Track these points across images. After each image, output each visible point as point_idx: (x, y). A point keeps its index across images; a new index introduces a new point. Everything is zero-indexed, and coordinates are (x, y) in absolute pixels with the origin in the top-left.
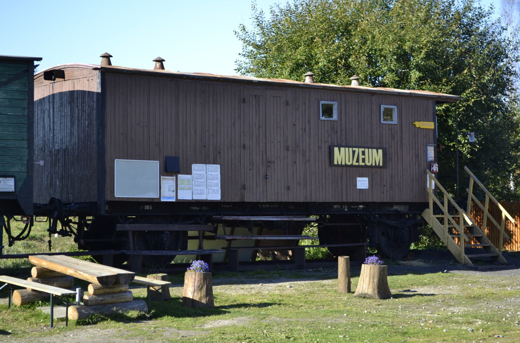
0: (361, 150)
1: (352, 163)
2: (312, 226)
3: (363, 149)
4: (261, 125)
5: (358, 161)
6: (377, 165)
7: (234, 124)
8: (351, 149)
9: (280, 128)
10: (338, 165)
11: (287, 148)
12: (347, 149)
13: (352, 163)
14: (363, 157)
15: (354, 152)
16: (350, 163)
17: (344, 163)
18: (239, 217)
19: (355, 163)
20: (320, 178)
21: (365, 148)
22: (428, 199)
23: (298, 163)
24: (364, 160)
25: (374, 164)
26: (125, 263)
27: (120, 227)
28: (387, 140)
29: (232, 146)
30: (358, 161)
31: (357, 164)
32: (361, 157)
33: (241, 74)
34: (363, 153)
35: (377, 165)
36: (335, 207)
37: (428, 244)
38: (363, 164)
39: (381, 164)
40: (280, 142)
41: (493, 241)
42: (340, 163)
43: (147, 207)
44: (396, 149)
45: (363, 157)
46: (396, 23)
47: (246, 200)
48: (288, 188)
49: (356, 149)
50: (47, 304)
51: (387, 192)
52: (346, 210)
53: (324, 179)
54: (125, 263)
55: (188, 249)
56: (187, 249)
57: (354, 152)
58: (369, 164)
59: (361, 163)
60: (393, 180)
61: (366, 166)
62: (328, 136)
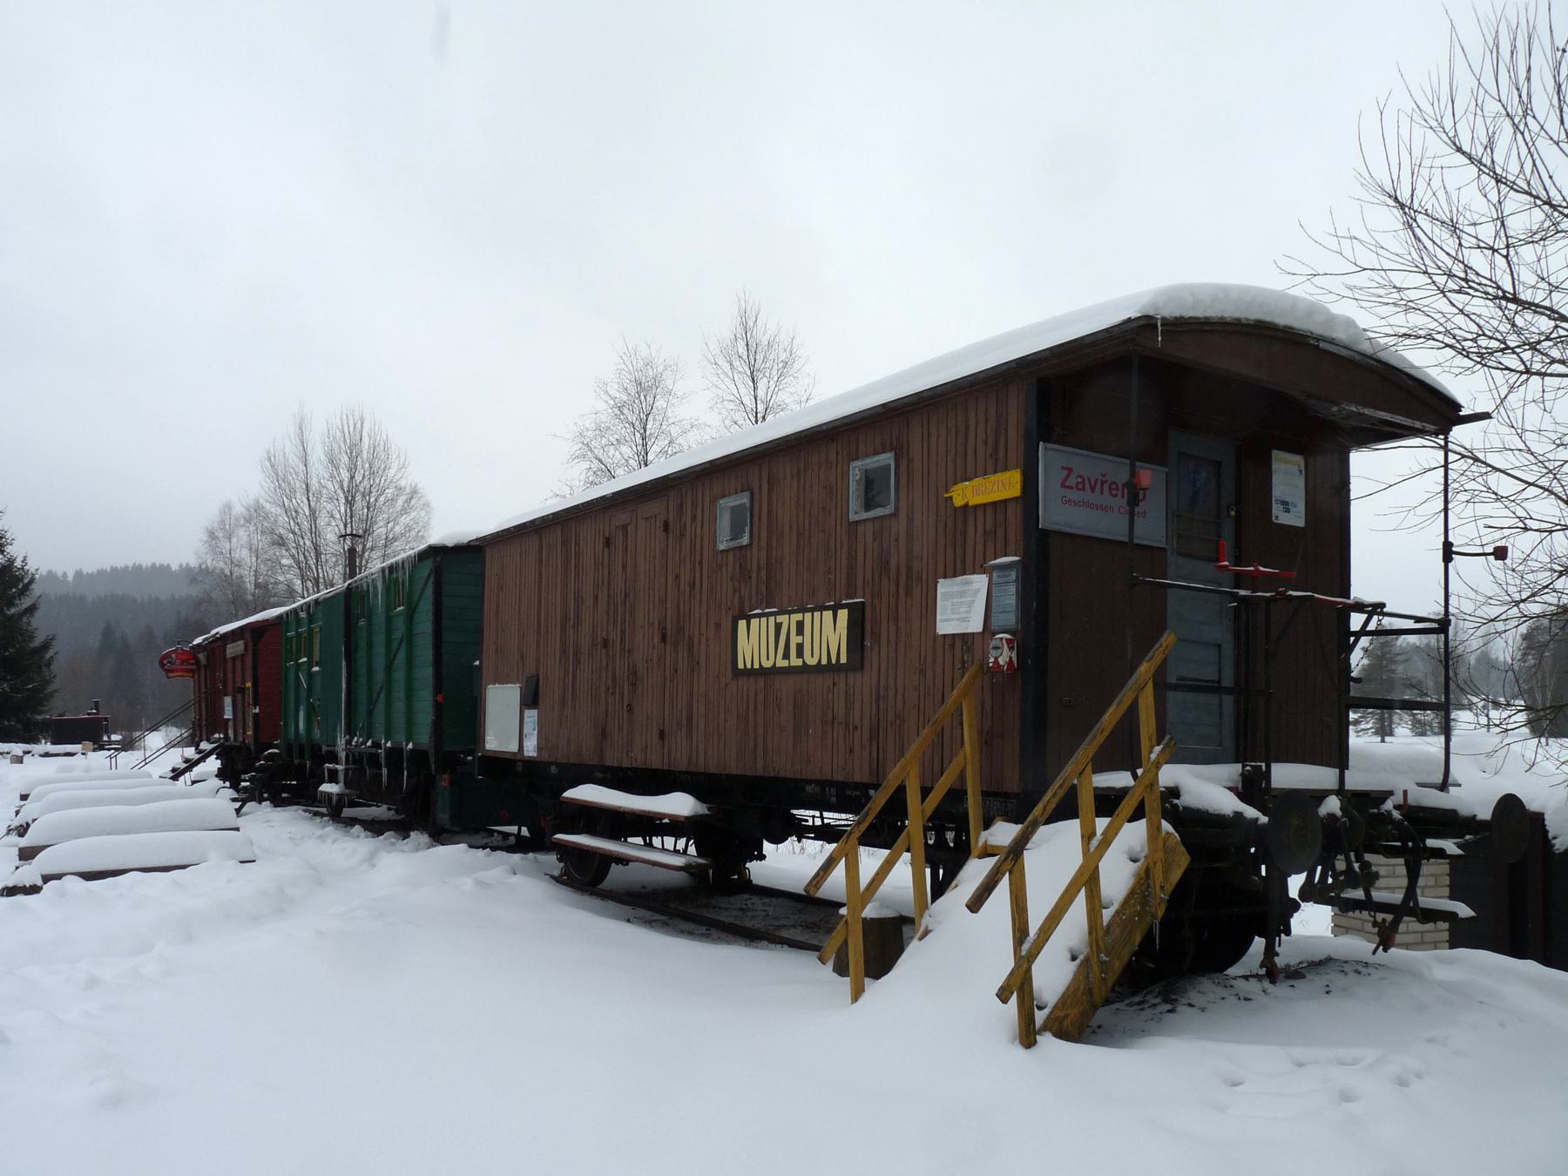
1: (775, 663)
3: (799, 617)
5: (786, 656)
6: (749, 666)
9: (654, 590)
11: (664, 638)
13: (775, 663)
14: (799, 640)
15: (778, 626)
19: (782, 663)
21: (803, 610)
22: (966, 787)
24: (800, 654)
25: (824, 662)
28: (868, 575)
30: (786, 656)
33: (1555, 446)
34: (800, 625)
35: (749, 666)
39: (843, 660)
40: (652, 625)
42: (756, 666)
44: (892, 600)
48: (662, 735)
49: (783, 619)
51: (862, 747)
55: (1097, 819)
56: (1097, 816)
57: (778, 626)
59: (795, 662)
60: (881, 707)
62: (735, 591)
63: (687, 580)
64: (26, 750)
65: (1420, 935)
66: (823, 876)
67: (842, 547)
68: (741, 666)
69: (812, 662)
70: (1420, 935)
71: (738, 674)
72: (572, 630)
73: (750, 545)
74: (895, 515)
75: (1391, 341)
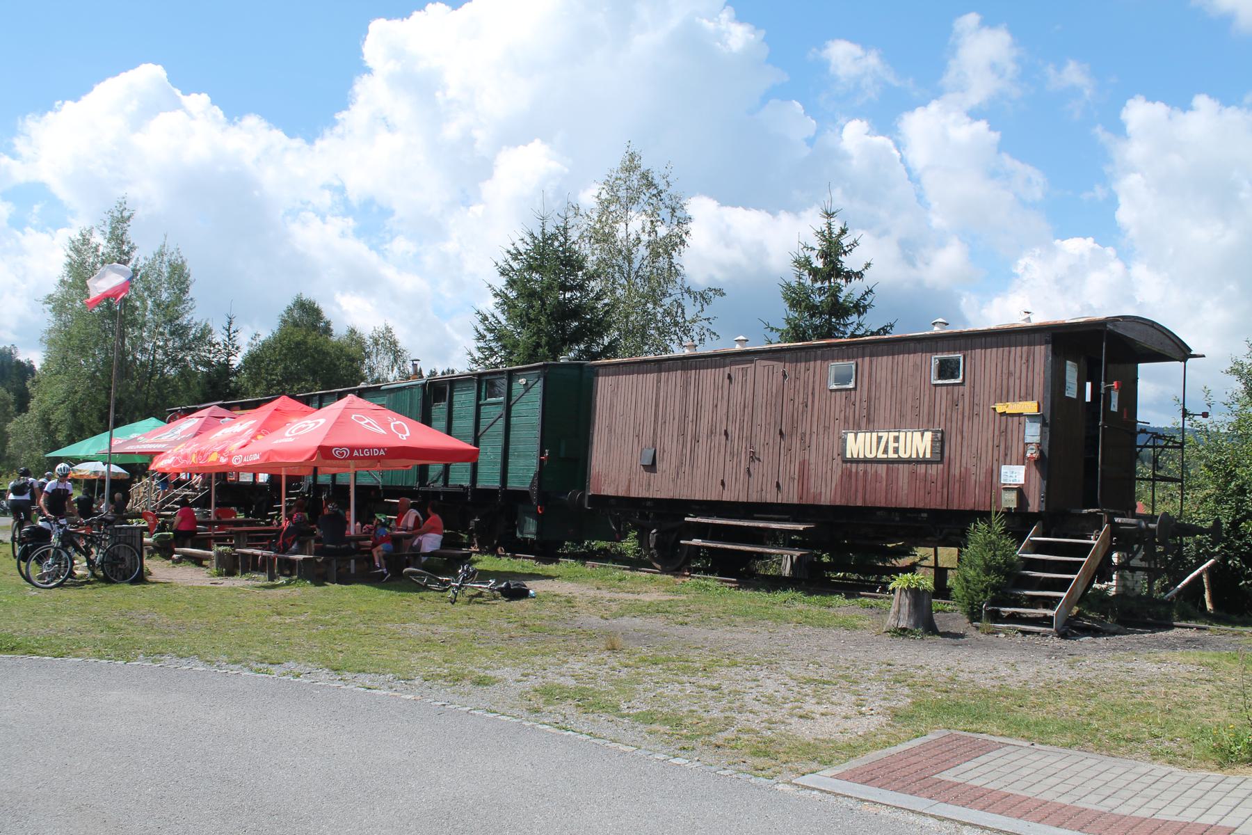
0: (892, 435)
5: (886, 451)
6: (921, 456)
7: (716, 406)
14: (896, 445)
15: (879, 438)
19: (881, 455)
23: (793, 450)
24: (896, 450)
26: (495, 542)
28: (943, 410)
29: (712, 433)
30: (886, 451)
31: (885, 456)
32: (892, 445)
34: (896, 439)
35: (921, 456)
36: (878, 513)
38: (896, 456)
39: (928, 456)
43: (925, 515)
45: (896, 445)
46: (943, 657)
49: (885, 435)
50: (450, 570)
52: (898, 519)
53: (829, 472)
54: (495, 542)
57: (879, 438)
58: (907, 456)
59: (892, 455)
63: (801, 400)
64: (472, 352)
65: (933, 565)
66: (620, 559)
67: (674, 419)
68: (849, 456)
69: (903, 455)
70: (933, 565)
71: (845, 461)
72: (690, 424)
73: (855, 389)
74: (962, 384)
75: (194, 446)
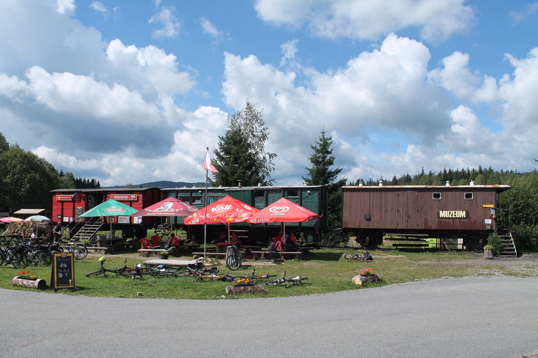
0: (454, 212)
2: (175, 231)
3: (455, 211)
4: (405, 202)
5: (452, 215)
6: (463, 217)
7: (393, 202)
8: (448, 212)
10: (442, 218)
12: (446, 211)
15: (450, 213)
16: (448, 217)
17: (445, 217)
18: (419, 244)
20: (360, 198)
24: (455, 215)
25: (461, 217)
27: (59, 231)
34: (455, 213)
35: (463, 217)
37: (535, 218)
39: (465, 217)
41: (219, 194)
47: (361, 228)
49: (451, 212)
57: (450, 213)
58: (458, 217)
59: (454, 216)
61: (456, 218)
